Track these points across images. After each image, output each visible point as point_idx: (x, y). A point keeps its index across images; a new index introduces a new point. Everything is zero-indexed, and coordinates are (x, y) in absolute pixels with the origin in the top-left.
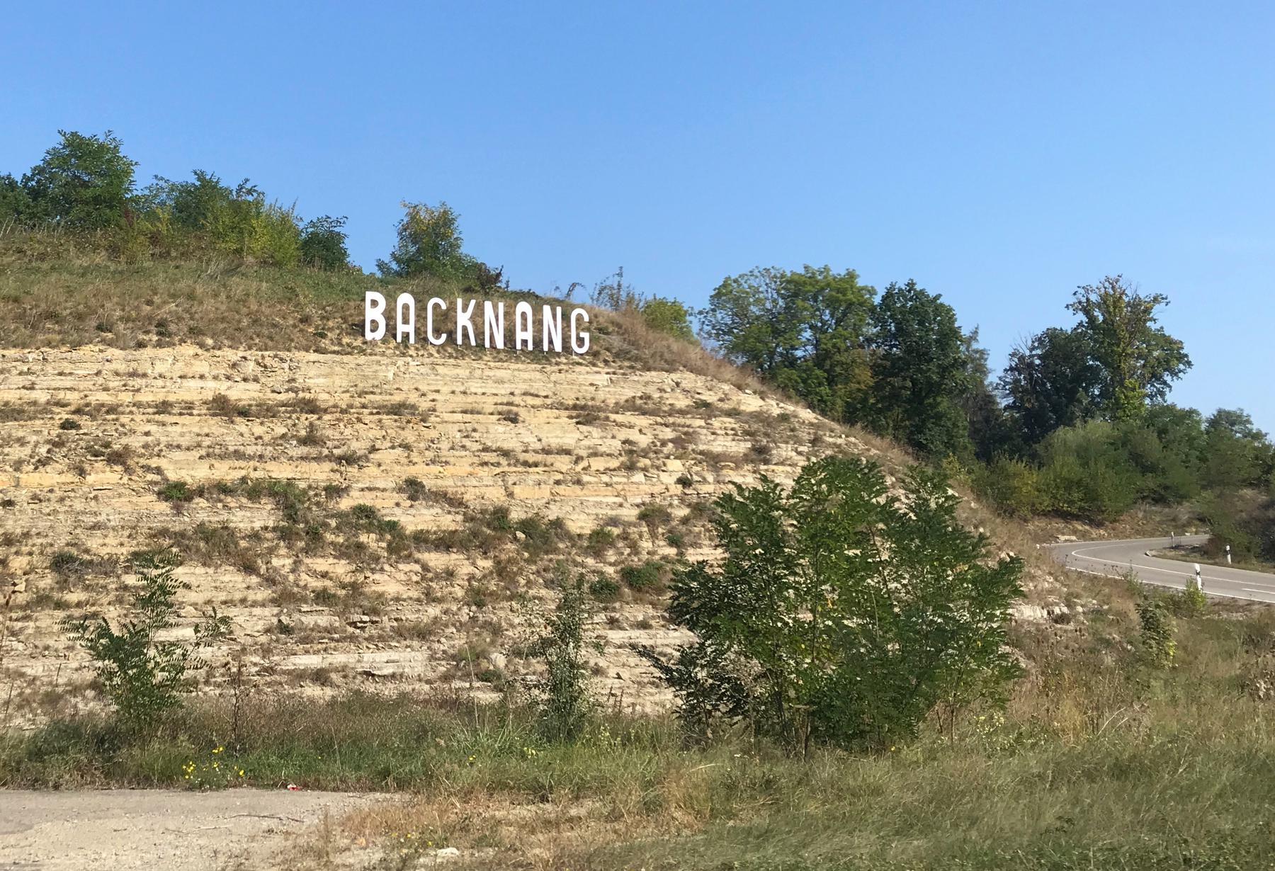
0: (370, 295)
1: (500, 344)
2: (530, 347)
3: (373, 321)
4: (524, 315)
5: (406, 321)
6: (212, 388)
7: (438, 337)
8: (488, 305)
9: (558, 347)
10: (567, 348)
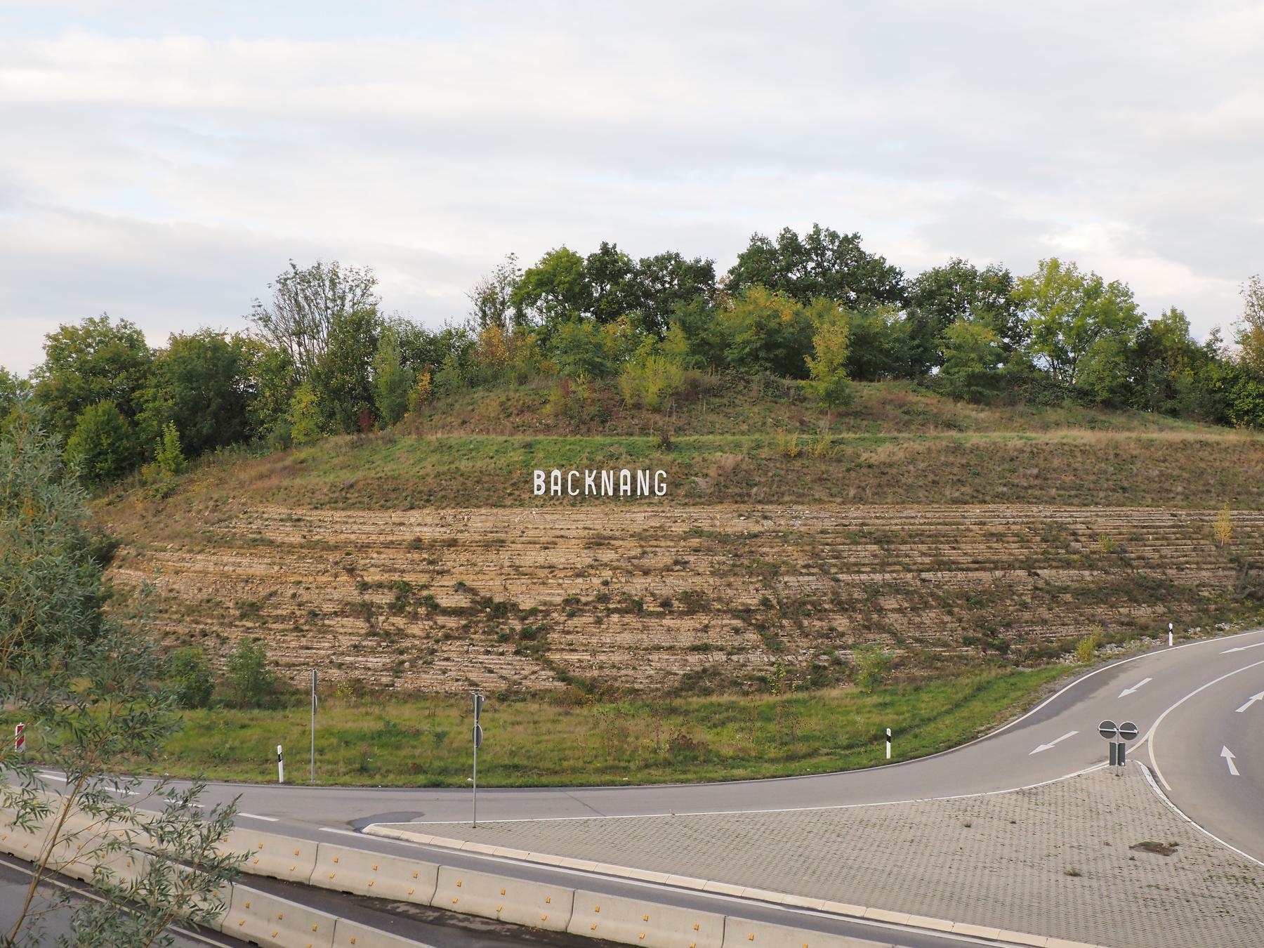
0: (536, 472)
5: (625, 484)
9: (646, 493)
10: (652, 492)
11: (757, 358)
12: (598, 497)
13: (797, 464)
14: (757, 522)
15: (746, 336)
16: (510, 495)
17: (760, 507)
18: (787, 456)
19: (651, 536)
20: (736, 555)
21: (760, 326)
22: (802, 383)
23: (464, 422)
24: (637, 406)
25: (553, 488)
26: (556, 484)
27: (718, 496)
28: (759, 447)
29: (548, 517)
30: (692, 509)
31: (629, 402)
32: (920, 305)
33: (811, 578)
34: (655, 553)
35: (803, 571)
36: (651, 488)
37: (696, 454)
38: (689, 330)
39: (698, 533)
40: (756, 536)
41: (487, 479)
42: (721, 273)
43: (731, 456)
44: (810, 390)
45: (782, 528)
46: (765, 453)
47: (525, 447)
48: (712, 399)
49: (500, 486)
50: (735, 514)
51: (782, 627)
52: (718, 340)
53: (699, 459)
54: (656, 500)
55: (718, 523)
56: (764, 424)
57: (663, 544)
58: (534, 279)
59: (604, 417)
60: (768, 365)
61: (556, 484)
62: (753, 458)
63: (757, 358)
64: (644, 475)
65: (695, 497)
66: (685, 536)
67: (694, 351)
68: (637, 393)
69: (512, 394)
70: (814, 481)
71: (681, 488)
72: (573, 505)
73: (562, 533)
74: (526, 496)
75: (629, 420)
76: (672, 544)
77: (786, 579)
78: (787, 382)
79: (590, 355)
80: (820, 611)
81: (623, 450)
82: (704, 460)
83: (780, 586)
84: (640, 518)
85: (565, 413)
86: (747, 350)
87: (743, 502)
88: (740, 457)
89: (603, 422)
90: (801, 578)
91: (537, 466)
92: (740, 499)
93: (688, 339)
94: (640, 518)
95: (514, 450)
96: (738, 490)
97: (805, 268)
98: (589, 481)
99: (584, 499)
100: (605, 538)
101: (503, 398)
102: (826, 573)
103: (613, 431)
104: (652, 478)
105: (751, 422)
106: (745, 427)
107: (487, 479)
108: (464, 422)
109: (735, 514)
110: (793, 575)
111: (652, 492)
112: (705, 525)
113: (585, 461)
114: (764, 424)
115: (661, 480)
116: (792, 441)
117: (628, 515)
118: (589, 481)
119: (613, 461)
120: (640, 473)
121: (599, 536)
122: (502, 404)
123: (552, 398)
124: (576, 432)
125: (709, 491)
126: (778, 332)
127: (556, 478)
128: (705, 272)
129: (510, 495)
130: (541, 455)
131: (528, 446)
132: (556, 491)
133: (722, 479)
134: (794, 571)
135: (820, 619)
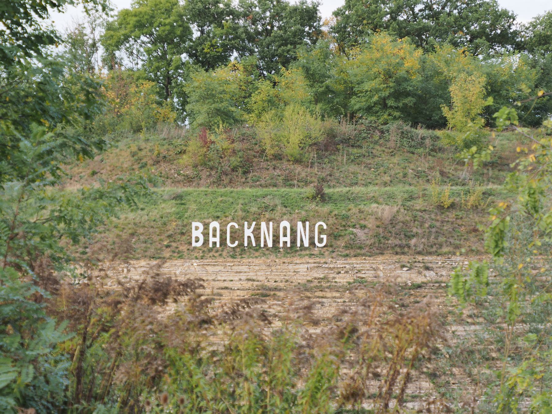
0: (194, 224)
1: (270, 244)
2: (289, 245)
5: (285, 235)
8: (263, 225)
9: (306, 244)
10: (312, 243)
11: (385, 106)
12: (256, 249)
13: (451, 215)
14: (420, 273)
15: (374, 84)
16: (167, 246)
17: (420, 258)
18: (441, 207)
19: (316, 287)
20: (403, 306)
21: (388, 75)
22: (438, 133)
23: (94, 173)
24: (278, 157)
25: (212, 239)
26: (214, 236)
27: (378, 248)
28: (411, 198)
29: (210, 269)
30: (353, 260)
31: (270, 151)
32: (531, 51)
33: (478, 327)
34: (322, 304)
35: (469, 320)
36: (312, 239)
37: (351, 206)
38: (312, 77)
39: (361, 282)
40: (419, 287)
41: (142, 231)
42: (327, 14)
43: (387, 208)
44: (447, 141)
45: (444, 279)
46: (419, 204)
47: (175, 198)
48: (351, 150)
49: (156, 238)
50: (398, 265)
51: (453, 375)
52: (342, 88)
53: (355, 210)
54: (316, 251)
55: (381, 274)
56: (405, 175)
57: (329, 295)
58: (133, 20)
59: (246, 168)
60: (397, 114)
61: (214, 236)
62: (408, 209)
63: (385, 106)
64: (304, 227)
65: (354, 249)
66: (350, 288)
67: (318, 98)
68: (277, 141)
69: (143, 145)
70: (469, 232)
71: (341, 240)
72: (233, 257)
73: (226, 284)
74: (183, 248)
75: (271, 171)
76: (338, 295)
77: (454, 328)
78: (421, 131)
79: (225, 104)
80: (487, 359)
81: (278, 201)
82: (361, 212)
83: (448, 336)
84: (302, 270)
85: (204, 164)
86: (375, 98)
87: (403, 253)
88: (395, 209)
89: (245, 173)
90: (467, 328)
91: (193, 218)
92: (401, 250)
93: (312, 86)
94: (302, 270)
95: (164, 201)
96: (397, 242)
97: (412, 10)
98: (248, 232)
99: (243, 250)
100: (270, 289)
101: (134, 148)
102: (492, 322)
103: (255, 183)
104: (312, 231)
105: (392, 172)
106: (387, 178)
107: (142, 231)
108: (94, 173)
109: (398, 265)
110: (460, 324)
111: (312, 243)
112: (369, 275)
113: (240, 213)
114: (405, 175)
115: (321, 231)
116: (446, 192)
117: (290, 267)
118: (248, 232)
119: (266, 211)
120: (300, 224)
121: (264, 287)
122: (133, 155)
123: (190, 149)
124: (218, 182)
125: (368, 242)
126: (406, 80)
127: (215, 230)
128: (309, 15)
129: (167, 246)
130: (193, 206)
131: (178, 197)
132: (214, 243)
133: (381, 230)
134: (461, 321)
135: (490, 368)
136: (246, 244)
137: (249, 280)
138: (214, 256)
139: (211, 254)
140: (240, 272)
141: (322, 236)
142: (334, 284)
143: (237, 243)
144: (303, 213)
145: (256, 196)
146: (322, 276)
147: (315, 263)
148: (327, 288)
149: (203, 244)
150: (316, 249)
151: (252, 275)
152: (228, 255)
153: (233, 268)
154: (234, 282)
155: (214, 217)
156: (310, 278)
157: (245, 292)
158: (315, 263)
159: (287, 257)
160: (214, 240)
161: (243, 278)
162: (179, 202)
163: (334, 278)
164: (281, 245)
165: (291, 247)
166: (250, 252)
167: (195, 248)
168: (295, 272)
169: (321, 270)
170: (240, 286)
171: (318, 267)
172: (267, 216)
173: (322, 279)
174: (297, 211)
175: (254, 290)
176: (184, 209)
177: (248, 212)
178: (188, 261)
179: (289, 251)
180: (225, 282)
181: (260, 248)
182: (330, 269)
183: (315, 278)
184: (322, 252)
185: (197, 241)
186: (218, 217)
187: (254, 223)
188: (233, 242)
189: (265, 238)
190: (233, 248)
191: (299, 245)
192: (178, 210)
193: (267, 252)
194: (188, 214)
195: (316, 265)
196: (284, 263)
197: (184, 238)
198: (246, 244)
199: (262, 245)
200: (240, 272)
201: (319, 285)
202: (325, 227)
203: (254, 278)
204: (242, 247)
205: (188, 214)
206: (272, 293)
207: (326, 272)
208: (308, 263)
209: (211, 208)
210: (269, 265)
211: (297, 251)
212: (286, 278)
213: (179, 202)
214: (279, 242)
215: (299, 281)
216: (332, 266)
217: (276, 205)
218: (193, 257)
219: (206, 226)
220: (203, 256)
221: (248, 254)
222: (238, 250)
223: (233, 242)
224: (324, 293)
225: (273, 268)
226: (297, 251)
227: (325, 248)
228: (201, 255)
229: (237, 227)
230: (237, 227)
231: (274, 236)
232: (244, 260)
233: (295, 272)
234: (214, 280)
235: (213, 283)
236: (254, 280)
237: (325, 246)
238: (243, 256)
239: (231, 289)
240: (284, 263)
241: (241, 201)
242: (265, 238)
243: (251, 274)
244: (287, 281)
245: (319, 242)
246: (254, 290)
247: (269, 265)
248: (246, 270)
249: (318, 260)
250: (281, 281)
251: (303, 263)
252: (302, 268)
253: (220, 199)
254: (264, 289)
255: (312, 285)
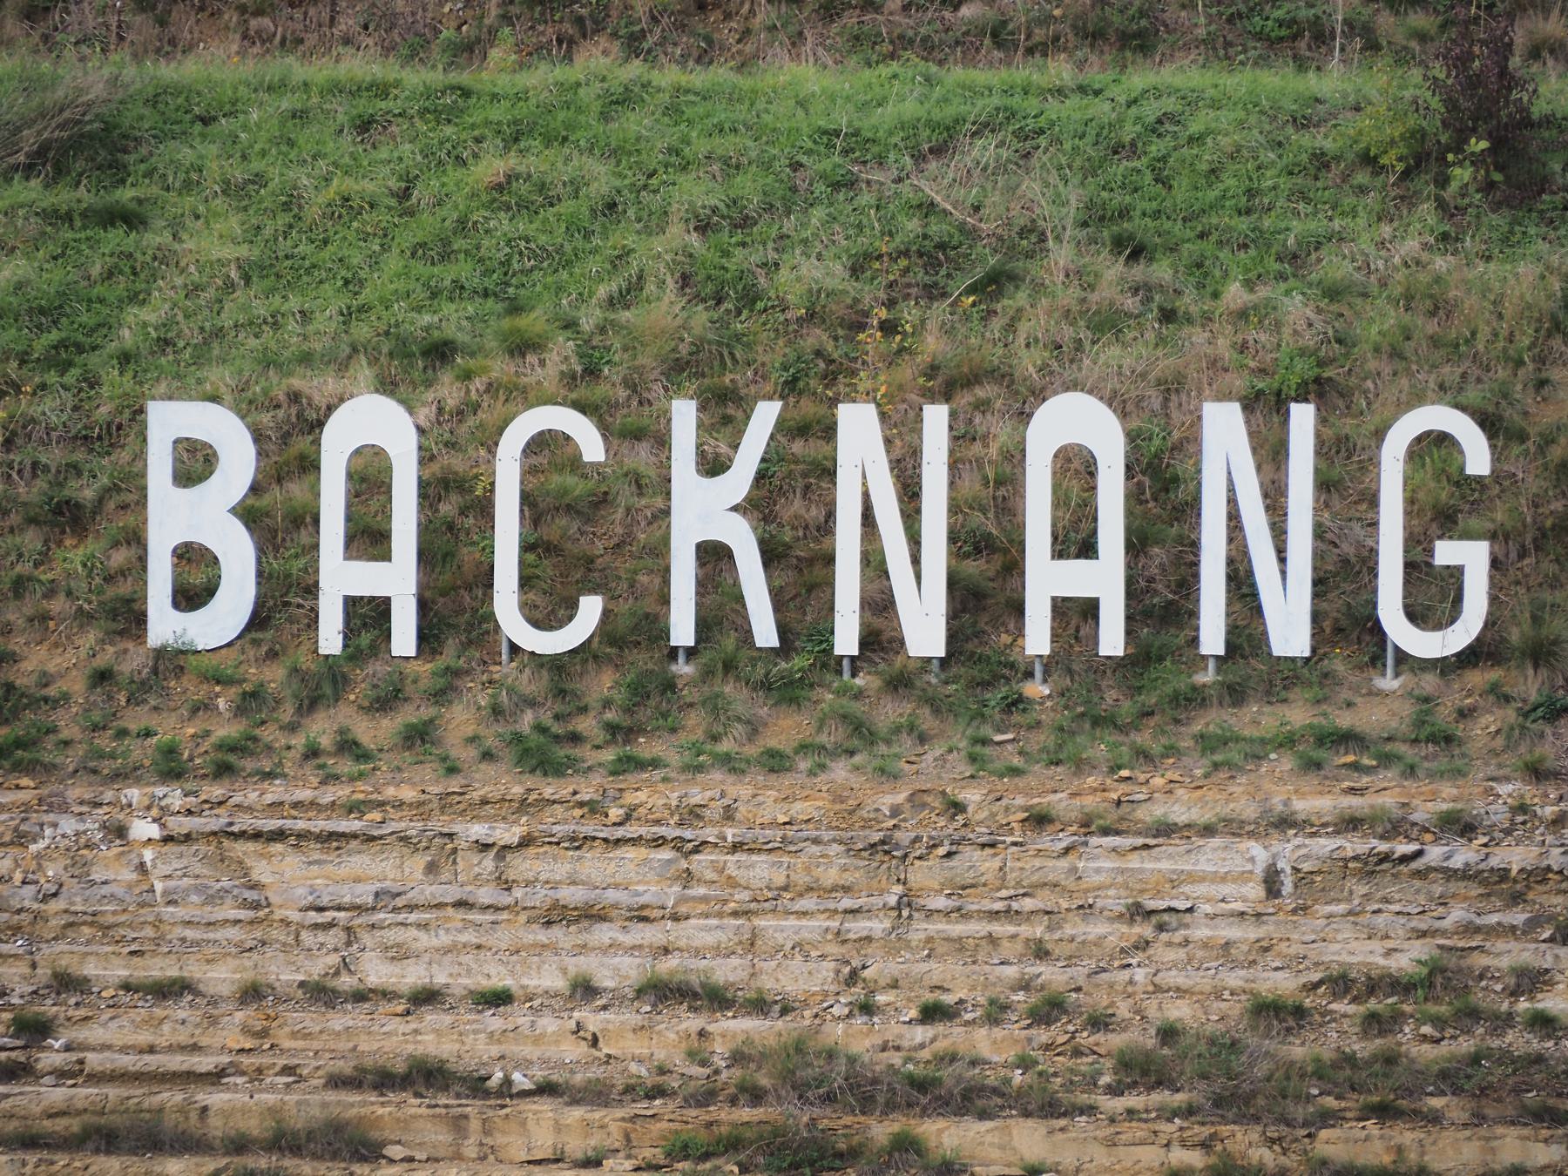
0: (170, 421)
1: (924, 629)
2: (1112, 640)
3: (190, 555)
4: (1076, 468)
5: (1076, 541)
6: (570, 828)
7: (547, 617)
8: (859, 432)
9: (1289, 628)
10: (1346, 621)
12: (789, 673)
19: (1340, 1073)
25: (341, 577)
26: (369, 539)
29: (288, 876)
36: (1342, 578)
54: (1382, 704)
61: (369, 539)
64: (1271, 453)
72: (542, 756)
73: (432, 1037)
81: (1051, 195)
91: (178, 361)
98: (705, 510)
99: (652, 697)
113: (664, 309)
115: (1444, 504)
117: (1101, 863)
118: (705, 510)
119: (942, 307)
120: (1224, 432)
127: (369, 479)
130: (217, 242)
136: (682, 631)
137: (663, 993)
138: (348, 746)
139: (322, 728)
140: (591, 915)
141: (1447, 552)
142: (1519, 1041)
143: (591, 609)
144: (1296, 308)
145: (857, 144)
146: (1407, 959)
147: (1351, 824)
148: (1449, 1078)
149: (258, 620)
150: (1388, 682)
151: (703, 946)
152: (492, 735)
153: (523, 866)
154: (518, 1016)
155: (402, 350)
156: (1280, 983)
157: (612, 1119)
158: (1351, 824)
159: (1081, 766)
160: (367, 579)
161: (617, 970)
162: (84, 196)
163: (1531, 980)
164: (1038, 638)
165: (1140, 659)
166: (715, 706)
167: (173, 660)
168: (1138, 912)
169: (1405, 895)
170: (573, 1051)
171: (1373, 866)
172: (933, 344)
173: (1401, 986)
174: (1235, 294)
175: (706, 1097)
176: (125, 265)
177: (750, 298)
178: (76, 791)
179: (1111, 696)
180: (431, 1018)
181: (828, 662)
182: (1501, 885)
183: (1340, 984)
184: (1444, 715)
185: (191, 597)
186: (440, 352)
187: (766, 415)
188: (548, 610)
189: (874, 563)
190: (557, 665)
191: (1212, 637)
192: (50, 280)
193: (889, 712)
194: (150, 315)
195: (1354, 845)
196: (1040, 820)
197: (74, 556)
198: (682, 631)
199: (846, 641)
200: (591, 915)
201: (1363, 1048)
202: (1478, 457)
203: (727, 971)
204: (642, 660)
205: (150, 315)
206: (881, 1130)
207: (1457, 914)
208: (1285, 823)
209: (393, 263)
210: (882, 848)
211: (1195, 699)
212: (1052, 975)
213: (84, 196)
214: (1018, 608)
215: (1180, 1011)
216: (1515, 856)
217: (1034, 236)
218: (139, 752)
219: (289, 447)
220: (242, 747)
221: (695, 723)
222: (603, 684)
223: (548, 610)
224: (1407, 1136)
225: (922, 874)
226: (1195, 699)
227: (1478, 678)
228: (227, 730)
229: (591, 444)
230: (591, 444)
231: (964, 543)
232: (645, 794)
233: (1138, 912)
234: (321, 994)
235: (310, 1019)
236: (717, 999)
237: (1470, 657)
238: (645, 748)
239: (477, 1086)
240: (1040, 820)
241: (696, 192)
242: (874, 563)
243: (698, 932)
244: (1050, 1010)
245: (1416, 615)
246: (706, 1097)
247: (882, 848)
248: (650, 892)
249: (1385, 794)
250: (996, 1013)
251: (1233, 828)
252: (1220, 877)
253: (492, 166)
254: (801, 1090)
255: (1298, 1050)
